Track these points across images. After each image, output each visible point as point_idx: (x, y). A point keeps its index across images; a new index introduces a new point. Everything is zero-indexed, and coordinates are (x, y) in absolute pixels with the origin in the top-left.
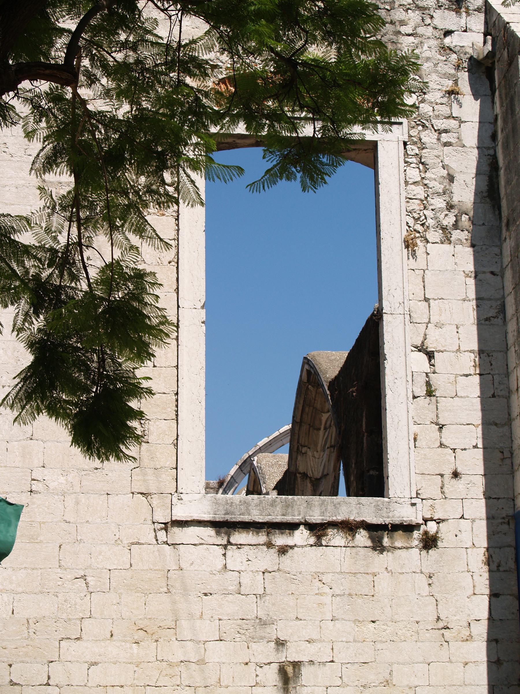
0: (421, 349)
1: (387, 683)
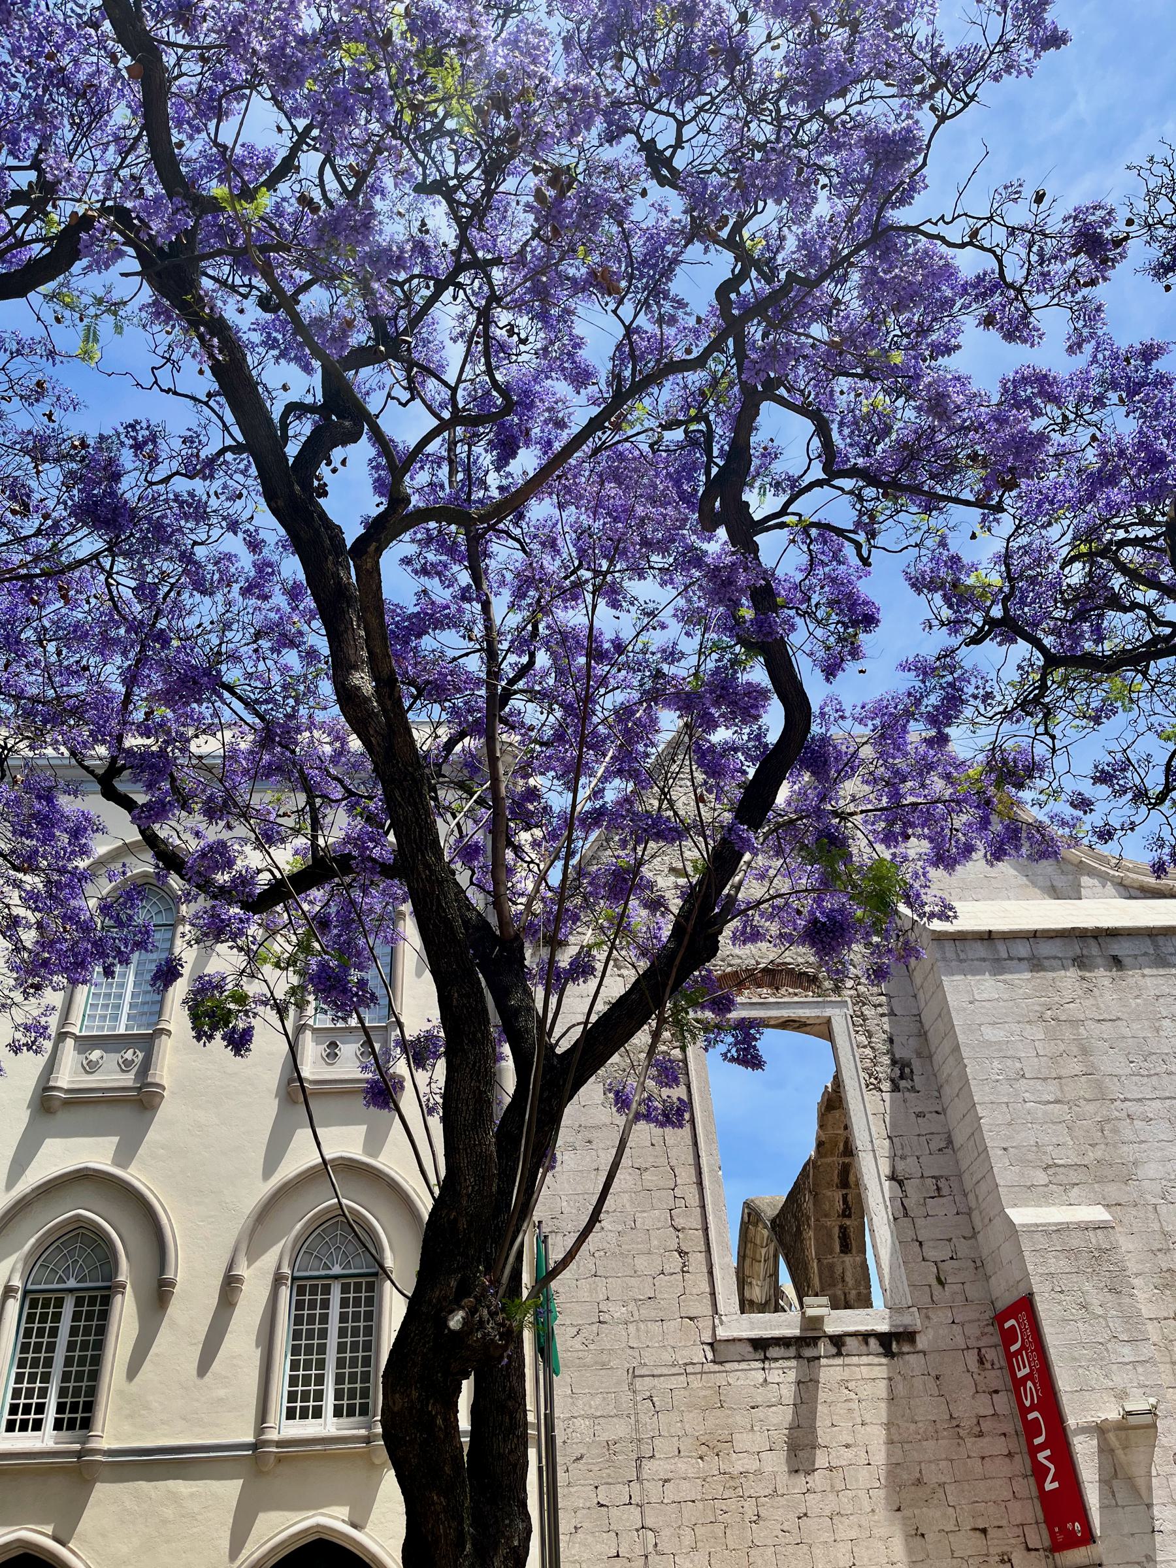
0: (1002, 1561)
1: (919, 1482)
